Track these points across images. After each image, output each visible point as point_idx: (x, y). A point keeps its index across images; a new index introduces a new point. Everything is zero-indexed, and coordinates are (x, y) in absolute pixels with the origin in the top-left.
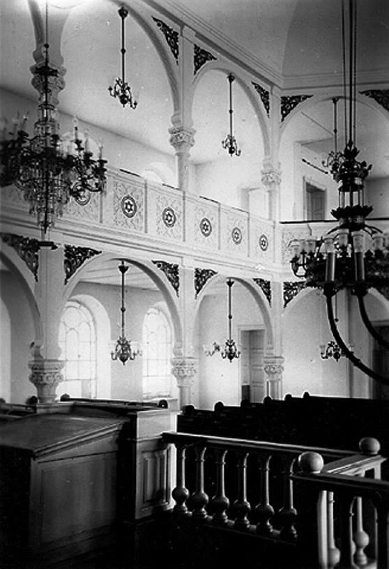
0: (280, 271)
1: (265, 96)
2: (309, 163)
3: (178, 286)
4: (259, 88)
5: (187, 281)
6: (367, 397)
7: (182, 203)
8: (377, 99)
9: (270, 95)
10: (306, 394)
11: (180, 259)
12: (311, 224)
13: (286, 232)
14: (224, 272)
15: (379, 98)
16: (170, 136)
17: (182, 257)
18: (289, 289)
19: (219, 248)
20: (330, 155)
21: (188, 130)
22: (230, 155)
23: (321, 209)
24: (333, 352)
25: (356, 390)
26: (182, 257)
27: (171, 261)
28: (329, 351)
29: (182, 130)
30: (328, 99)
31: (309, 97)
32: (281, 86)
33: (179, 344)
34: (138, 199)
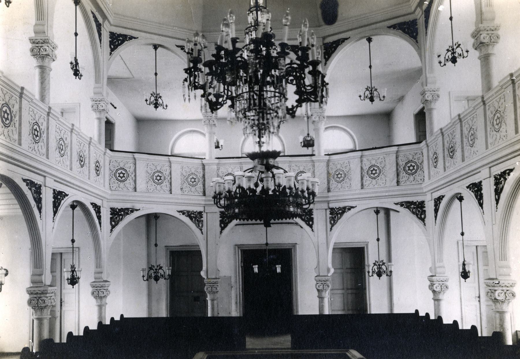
0: (203, 203)
1: (99, 26)
2: (189, 96)
3: (312, 224)
4: (96, 20)
5: (47, 198)
6: (290, 337)
7: (46, 119)
8: (404, 31)
9: (102, 27)
10: (122, 316)
11: (42, 178)
12: (137, 156)
13: (113, 160)
14: (73, 195)
15: (405, 28)
16: (30, 46)
17: (45, 177)
18: (116, 214)
19: (71, 169)
20: (152, 94)
21: (52, 45)
22: (75, 77)
23: (110, 140)
24: (153, 275)
25: (154, 309)
26: (45, 177)
27: (37, 179)
28: (150, 274)
29: (48, 43)
30: (150, 44)
31: (135, 38)
32: (112, 22)
33: (38, 271)
34: (13, 107)
